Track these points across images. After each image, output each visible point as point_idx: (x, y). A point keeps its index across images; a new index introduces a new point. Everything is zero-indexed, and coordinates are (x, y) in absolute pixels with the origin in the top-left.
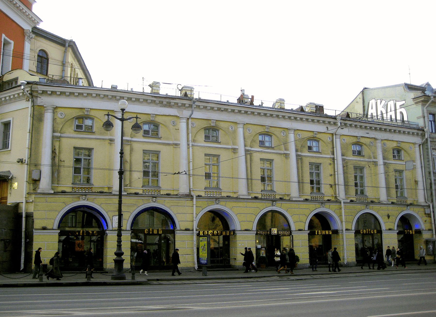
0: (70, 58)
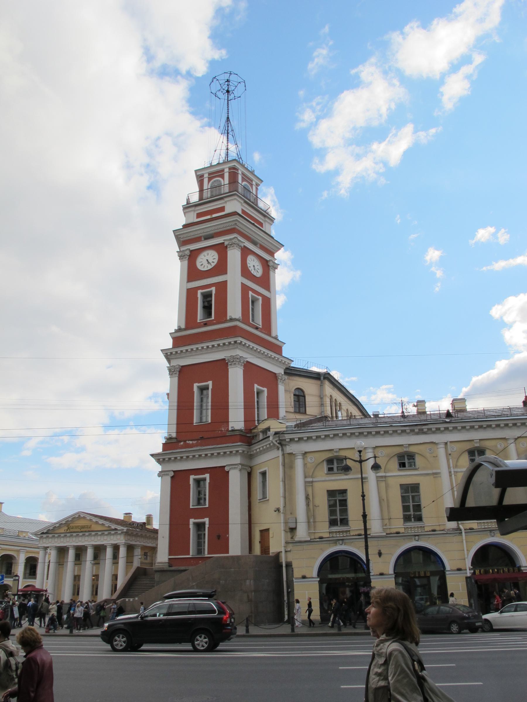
0: (329, 389)
